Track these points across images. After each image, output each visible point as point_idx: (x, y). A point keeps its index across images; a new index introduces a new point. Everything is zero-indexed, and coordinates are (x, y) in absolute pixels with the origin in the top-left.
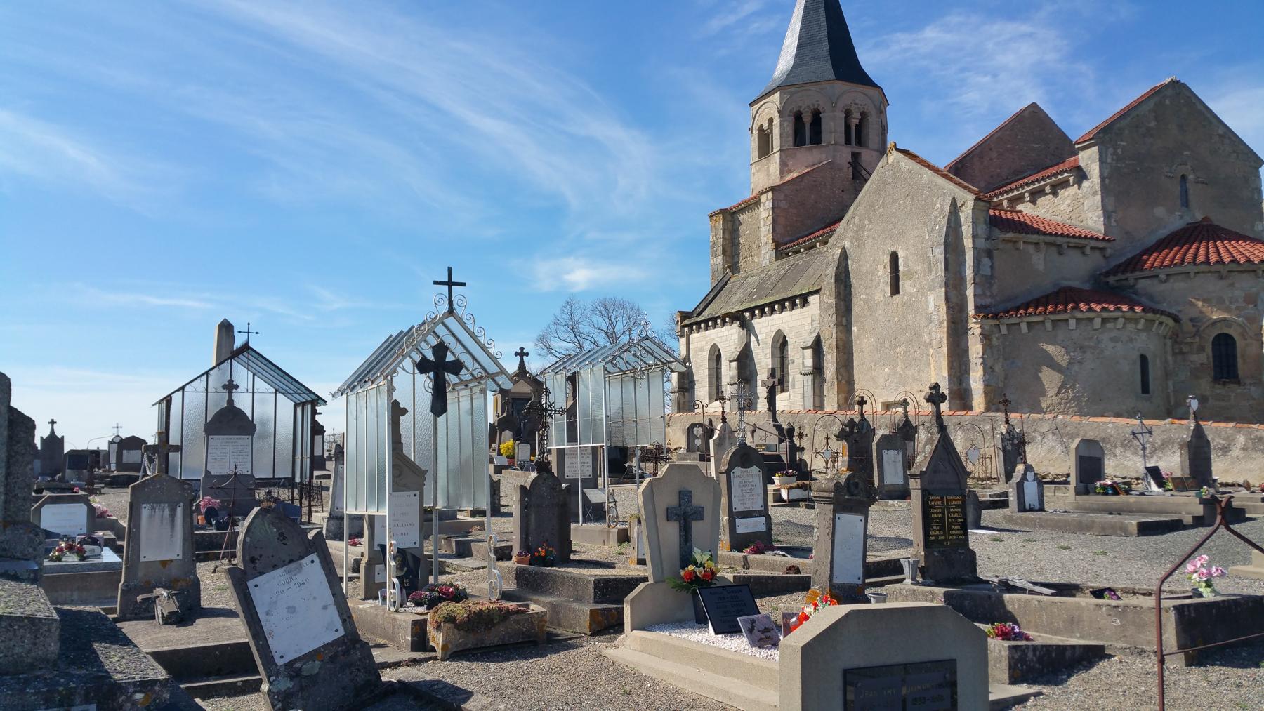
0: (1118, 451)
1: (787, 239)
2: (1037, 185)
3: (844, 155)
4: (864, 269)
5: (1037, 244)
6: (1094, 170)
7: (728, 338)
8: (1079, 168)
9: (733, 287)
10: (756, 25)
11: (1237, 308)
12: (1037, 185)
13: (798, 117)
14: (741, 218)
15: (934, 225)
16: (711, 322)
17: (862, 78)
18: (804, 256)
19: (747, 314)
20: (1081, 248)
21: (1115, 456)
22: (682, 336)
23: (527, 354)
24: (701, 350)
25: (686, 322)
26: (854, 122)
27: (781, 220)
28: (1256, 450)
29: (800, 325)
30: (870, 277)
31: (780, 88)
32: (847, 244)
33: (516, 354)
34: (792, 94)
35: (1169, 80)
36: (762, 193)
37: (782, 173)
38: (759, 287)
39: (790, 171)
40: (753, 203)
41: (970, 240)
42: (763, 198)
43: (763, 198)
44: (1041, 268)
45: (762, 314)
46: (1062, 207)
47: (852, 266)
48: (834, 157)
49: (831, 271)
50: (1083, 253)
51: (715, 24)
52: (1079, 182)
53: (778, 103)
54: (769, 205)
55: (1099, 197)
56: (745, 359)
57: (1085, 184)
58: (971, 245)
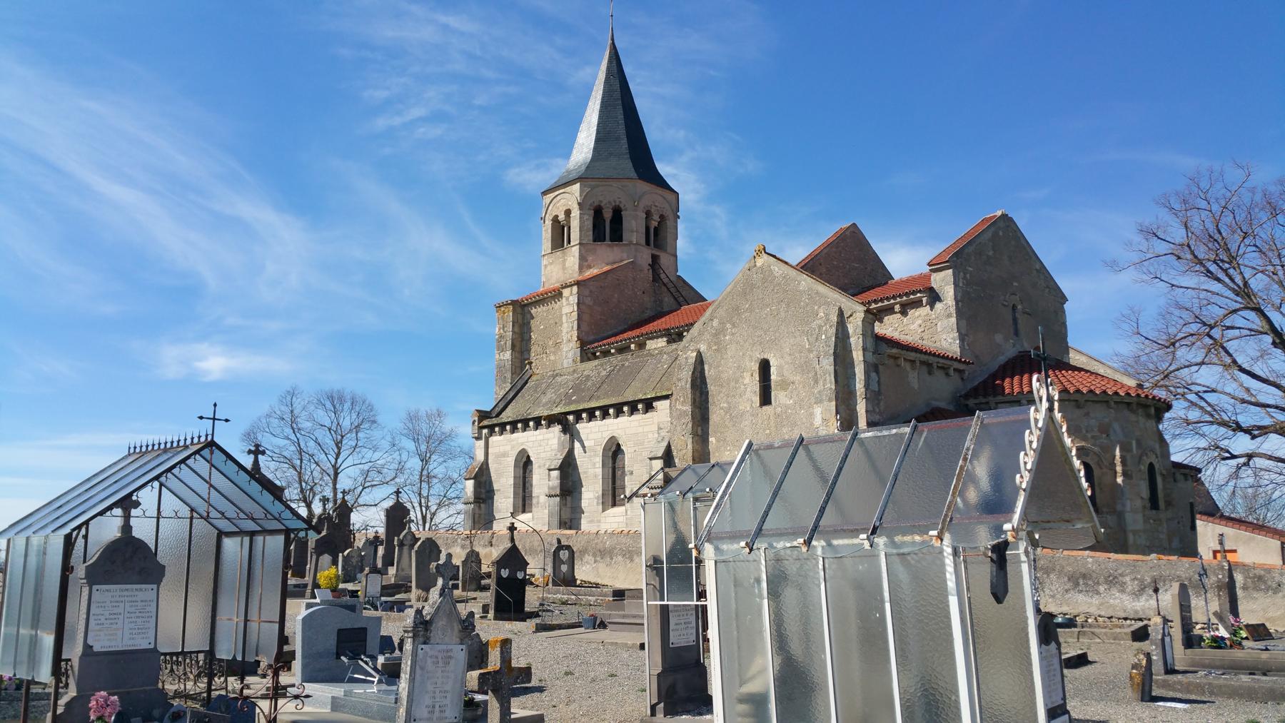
0: (1102, 589)
1: (591, 338)
2: (886, 303)
3: (645, 256)
4: (725, 376)
5: (913, 362)
6: (948, 293)
7: (544, 445)
8: (931, 289)
9: (537, 386)
10: (422, 130)
11: (1093, 437)
12: (886, 303)
13: (598, 212)
14: (533, 311)
15: (819, 335)
16: (523, 423)
17: (661, 182)
18: (628, 360)
19: (571, 418)
20: (944, 369)
21: (1098, 593)
22: (478, 438)
23: (263, 453)
24: (505, 455)
25: (486, 423)
26: (654, 224)
27: (586, 317)
28: (1257, 589)
29: (643, 435)
30: (733, 384)
31: (580, 179)
32: (703, 348)
33: (250, 452)
34: (593, 188)
35: (999, 213)
36: (567, 286)
37: (581, 268)
38: (577, 388)
39: (590, 267)
40: (556, 294)
41: (861, 353)
42: (566, 292)
43: (566, 292)
44: (916, 387)
45: (592, 416)
46: (912, 327)
47: (709, 372)
48: (635, 257)
49: (686, 375)
50: (947, 374)
51: (381, 123)
52: (932, 304)
53: (578, 194)
54: (574, 299)
55: (954, 320)
56: (568, 469)
57: (938, 306)
58: (861, 358)
